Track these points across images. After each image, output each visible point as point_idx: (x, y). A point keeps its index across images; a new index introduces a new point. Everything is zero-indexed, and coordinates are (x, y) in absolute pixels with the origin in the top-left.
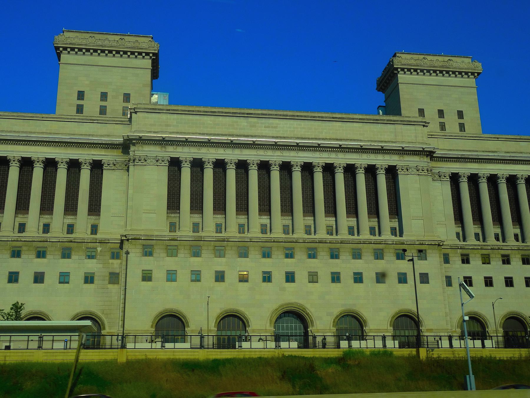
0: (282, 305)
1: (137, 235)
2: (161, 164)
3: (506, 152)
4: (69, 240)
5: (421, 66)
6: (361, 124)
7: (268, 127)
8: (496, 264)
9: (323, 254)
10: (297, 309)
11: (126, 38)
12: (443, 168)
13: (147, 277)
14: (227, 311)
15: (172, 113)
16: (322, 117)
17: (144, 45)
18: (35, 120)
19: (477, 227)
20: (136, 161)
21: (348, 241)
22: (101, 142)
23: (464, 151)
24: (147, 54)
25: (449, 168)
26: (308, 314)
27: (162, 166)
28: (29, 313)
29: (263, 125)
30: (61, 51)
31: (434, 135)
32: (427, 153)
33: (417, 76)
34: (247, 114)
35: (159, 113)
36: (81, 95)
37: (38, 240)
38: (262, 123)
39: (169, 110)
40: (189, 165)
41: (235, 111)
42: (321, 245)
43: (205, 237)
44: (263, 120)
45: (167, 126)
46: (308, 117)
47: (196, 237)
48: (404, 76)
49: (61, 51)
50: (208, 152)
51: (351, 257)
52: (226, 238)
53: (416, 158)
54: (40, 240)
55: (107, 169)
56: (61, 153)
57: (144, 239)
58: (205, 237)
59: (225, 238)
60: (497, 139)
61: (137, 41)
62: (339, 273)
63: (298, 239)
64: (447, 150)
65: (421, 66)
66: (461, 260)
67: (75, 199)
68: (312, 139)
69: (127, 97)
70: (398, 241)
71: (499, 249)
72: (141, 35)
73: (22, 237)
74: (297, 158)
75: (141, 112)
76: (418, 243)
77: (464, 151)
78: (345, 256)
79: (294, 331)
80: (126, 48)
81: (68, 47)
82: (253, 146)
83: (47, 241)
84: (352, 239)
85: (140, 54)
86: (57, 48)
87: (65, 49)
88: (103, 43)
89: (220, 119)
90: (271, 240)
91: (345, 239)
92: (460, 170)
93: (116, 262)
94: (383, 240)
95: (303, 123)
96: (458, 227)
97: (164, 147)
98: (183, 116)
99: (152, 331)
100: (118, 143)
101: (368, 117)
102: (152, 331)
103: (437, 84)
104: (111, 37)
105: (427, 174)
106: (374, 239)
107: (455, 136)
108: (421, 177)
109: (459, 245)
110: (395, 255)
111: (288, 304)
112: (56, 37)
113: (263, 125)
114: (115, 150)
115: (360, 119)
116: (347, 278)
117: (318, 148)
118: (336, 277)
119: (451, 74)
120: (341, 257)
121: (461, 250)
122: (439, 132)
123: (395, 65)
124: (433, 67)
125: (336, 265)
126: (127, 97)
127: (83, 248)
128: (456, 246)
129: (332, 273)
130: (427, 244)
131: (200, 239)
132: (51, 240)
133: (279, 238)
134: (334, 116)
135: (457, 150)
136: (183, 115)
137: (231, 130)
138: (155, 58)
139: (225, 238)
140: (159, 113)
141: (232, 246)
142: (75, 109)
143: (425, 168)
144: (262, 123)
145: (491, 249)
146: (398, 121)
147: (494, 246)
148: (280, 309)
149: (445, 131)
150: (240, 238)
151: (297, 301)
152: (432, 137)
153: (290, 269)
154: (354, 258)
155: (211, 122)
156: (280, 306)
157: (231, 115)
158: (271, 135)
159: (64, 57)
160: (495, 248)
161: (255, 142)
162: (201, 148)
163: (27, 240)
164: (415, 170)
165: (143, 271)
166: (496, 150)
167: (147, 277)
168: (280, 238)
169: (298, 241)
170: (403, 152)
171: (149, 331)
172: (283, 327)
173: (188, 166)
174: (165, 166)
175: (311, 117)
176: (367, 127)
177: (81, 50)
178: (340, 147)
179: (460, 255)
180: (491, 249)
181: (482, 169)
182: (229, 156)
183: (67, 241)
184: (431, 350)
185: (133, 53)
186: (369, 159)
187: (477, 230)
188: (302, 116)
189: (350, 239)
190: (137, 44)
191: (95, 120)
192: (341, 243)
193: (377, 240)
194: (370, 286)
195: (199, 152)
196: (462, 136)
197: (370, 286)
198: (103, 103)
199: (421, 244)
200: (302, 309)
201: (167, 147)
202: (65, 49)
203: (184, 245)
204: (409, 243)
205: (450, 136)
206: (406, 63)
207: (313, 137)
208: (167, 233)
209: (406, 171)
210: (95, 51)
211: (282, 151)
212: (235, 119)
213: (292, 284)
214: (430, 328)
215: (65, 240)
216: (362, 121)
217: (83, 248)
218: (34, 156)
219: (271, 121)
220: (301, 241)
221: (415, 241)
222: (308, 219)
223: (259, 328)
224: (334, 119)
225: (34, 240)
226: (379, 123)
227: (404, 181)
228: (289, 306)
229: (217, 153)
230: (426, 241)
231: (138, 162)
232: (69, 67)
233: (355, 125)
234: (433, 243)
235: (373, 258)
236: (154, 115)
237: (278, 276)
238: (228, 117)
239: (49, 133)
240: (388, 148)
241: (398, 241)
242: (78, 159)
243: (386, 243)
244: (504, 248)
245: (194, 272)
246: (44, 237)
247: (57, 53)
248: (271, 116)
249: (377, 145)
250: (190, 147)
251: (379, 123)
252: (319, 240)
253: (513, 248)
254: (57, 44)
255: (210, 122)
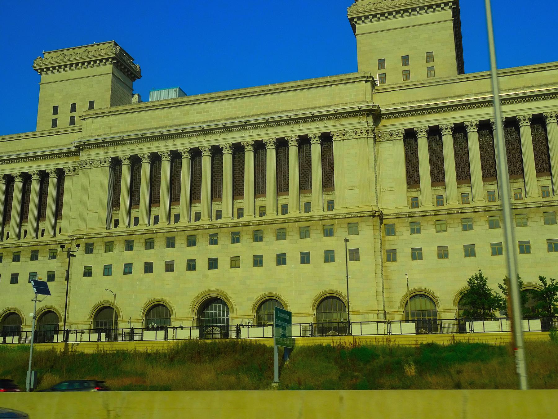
0: (204, 292)
1: (79, 235)
2: (85, 168)
3: (476, 94)
4: (36, 244)
5: (381, 10)
6: (295, 92)
7: (200, 113)
8: (480, 229)
9: (247, 237)
10: (203, 298)
11: (89, 49)
12: (395, 125)
13: (88, 272)
14: (266, 295)
15: (113, 115)
16: (252, 92)
17: (104, 52)
18: (15, 140)
19: (440, 188)
20: (83, 166)
21: (271, 221)
22: (60, 152)
23: (418, 101)
24: (107, 60)
25: (403, 124)
26: (228, 300)
27: (104, 167)
28: (6, 310)
29: (196, 112)
30: (356, 22)
31: (385, 89)
32: (366, 112)
33: (410, 17)
34: (180, 103)
35: (331, 85)
36: (56, 110)
37: (13, 246)
38: (194, 110)
39: (110, 112)
40: (148, 160)
41: (294, 84)
42: (245, 228)
43: (135, 231)
44: (196, 107)
45: (111, 127)
46: (238, 95)
47: (128, 232)
48: (364, 25)
49: (356, 22)
50: (144, 147)
51: (275, 238)
52: (310, 217)
53: (355, 120)
54: (15, 246)
55: (68, 176)
56: (33, 167)
57: (85, 238)
58: (135, 231)
59: (153, 230)
60: (382, 91)
61: (98, 49)
62: (262, 256)
63: (221, 224)
64: (400, 103)
65: (381, 10)
66: (409, 230)
67: (117, 199)
68: (242, 117)
69: (91, 105)
70: (325, 216)
71: (458, 213)
72: (104, 42)
73: (2, 244)
74: (226, 140)
75: (204, 102)
76: (348, 216)
77: (418, 101)
78: (293, 235)
79: (213, 318)
80: (388, 9)
81: (362, 16)
82: (182, 134)
83: (20, 246)
84: (276, 219)
85: (382, 15)
86: (351, 20)
87: (359, 18)
88: (367, 9)
89: (156, 113)
90: (196, 227)
91: (270, 219)
92: (416, 124)
93: (499, 231)
94: (309, 217)
95: (234, 103)
96: (416, 191)
97: (107, 148)
98: (124, 116)
99: (252, 316)
100: (74, 150)
101: (302, 83)
102: (252, 316)
103: (403, 26)
104: (78, 51)
105: (366, 136)
106: (299, 217)
107: (412, 85)
108: (360, 140)
109: (407, 213)
110: (322, 231)
111: (209, 291)
112: (35, 61)
113: (196, 112)
114: (75, 157)
115: (292, 87)
116: (270, 260)
117: (313, 118)
118: (259, 260)
119: (427, 10)
120: (264, 239)
121: (410, 219)
122: (401, 83)
123: (349, 15)
124: (395, 8)
125: (259, 248)
126: (91, 105)
127: (47, 250)
128: (404, 215)
129: (255, 257)
130: (360, 217)
131: (132, 233)
132: (23, 245)
133: (202, 225)
134: (267, 88)
135: (413, 102)
136: (124, 115)
137: (165, 122)
138: (455, 6)
139: (153, 230)
140: (331, 85)
141: (160, 238)
142: (51, 123)
143: (364, 130)
144: (194, 110)
145: (448, 214)
146: (334, 81)
147: (451, 210)
148: (202, 296)
149: (386, 83)
150: (167, 229)
151: (218, 288)
152: (384, 91)
153: (213, 256)
154: (277, 239)
155: (148, 117)
156: (202, 294)
157: (165, 107)
158: (202, 120)
159: (360, 27)
160: (453, 212)
161: (361, 108)
162: (138, 144)
163: (6, 247)
164: (353, 134)
165: (232, 258)
166: (464, 93)
167: (88, 272)
168: (204, 225)
169: (222, 226)
170: (337, 115)
171: (87, 322)
172: (211, 313)
173: (146, 161)
174: (107, 166)
175: (241, 94)
176: (301, 94)
177: (439, 5)
178: (268, 122)
179: (408, 225)
180: (448, 214)
181: (443, 119)
182: (162, 148)
183: (34, 244)
184: (76, 344)
185: (390, 13)
186: (153, 147)
187: (440, 192)
188: (232, 95)
189: (273, 219)
190: (98, 53)
191: (58, 132)
192: (243, 225)
193: (328, 216)
194: (293, 267)
195: (136, 148)
196: (420, 84)
197: (293, 267)
198: (406, 68)
199: (352, 217)
200: (223, 295)
201: (109, 148)
202: (359, 18)
203: (119, 241)
204: (339, 217)
205: (405, 86)
206: (362, 10)
207: (244, 115)
208: (105, 230)
209: (342, 136)
210: (406, 11)
211: (212, 136)
212: (169, 110)
213: (214, 271)
214: (357, 310)
215: (33, 244)
216: (294, 89)
217: (47, 250)
218: (519, 115)
219: (203, 106)
220: (224, 226)
221: (344, 214)
222: (241, 202)
223: (181, 316)
224: (264, 92)
225: (10, 246)
226: (314, 87)
227: (338, 147)
228: (211, 293)
229: (309, 128)
230: (357, 213)
231: (336, 138)
232: (47, 85)
233: (288, 94)
234: (366, 215)
235: (322, 235)
236: (99, 119)
237: (202, 264)
238: (163, 110)
239: (25, 150)
240: (219, 127)
241: (325, 216)
242: (438, 126)
243: (313, 219)
244: (464, 211)
245: (234, 259)
246: (17, 243)
247: (351, 26)
248: (202, 100)
249: (329, 110)
250: (318, 122)
251: (314, 87)
252: (241, 224)
253: (477, 210)
254: (35, 67)
255: (147, 117)
